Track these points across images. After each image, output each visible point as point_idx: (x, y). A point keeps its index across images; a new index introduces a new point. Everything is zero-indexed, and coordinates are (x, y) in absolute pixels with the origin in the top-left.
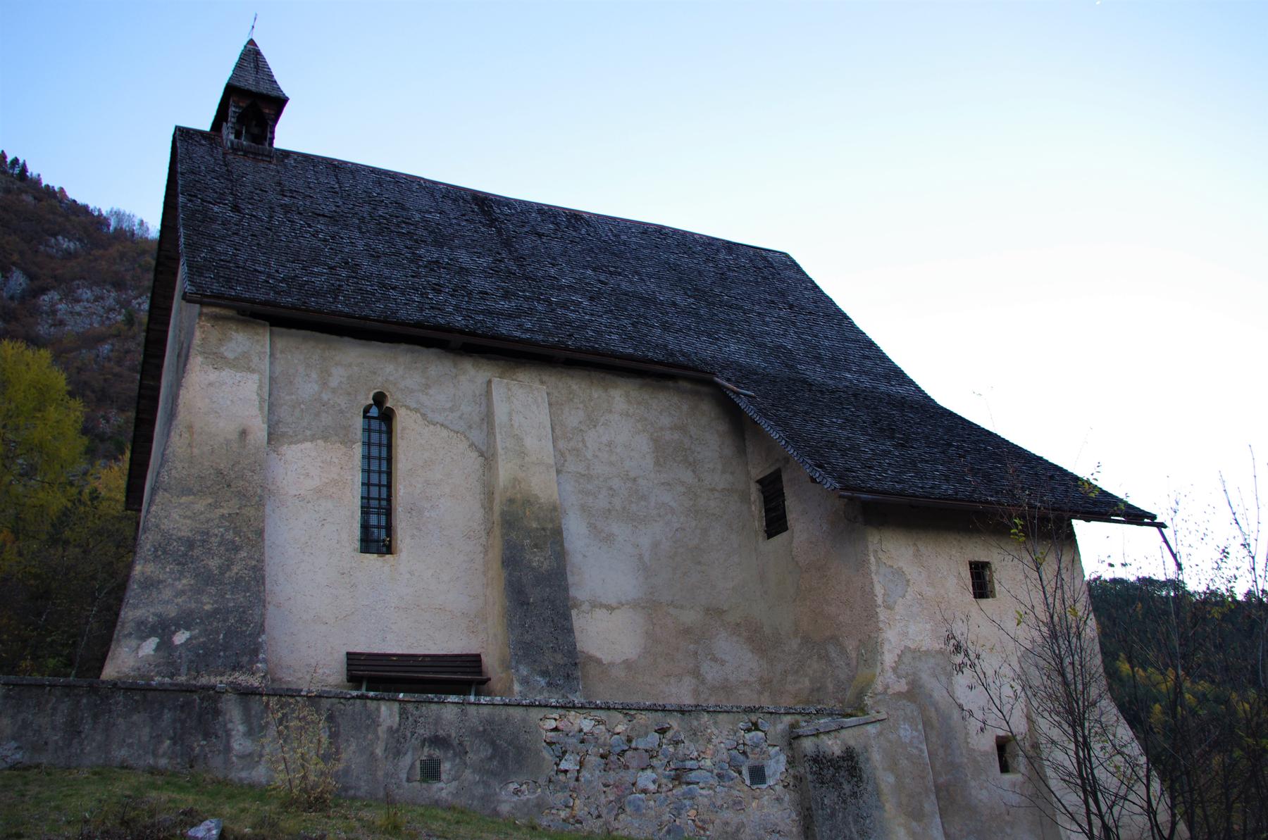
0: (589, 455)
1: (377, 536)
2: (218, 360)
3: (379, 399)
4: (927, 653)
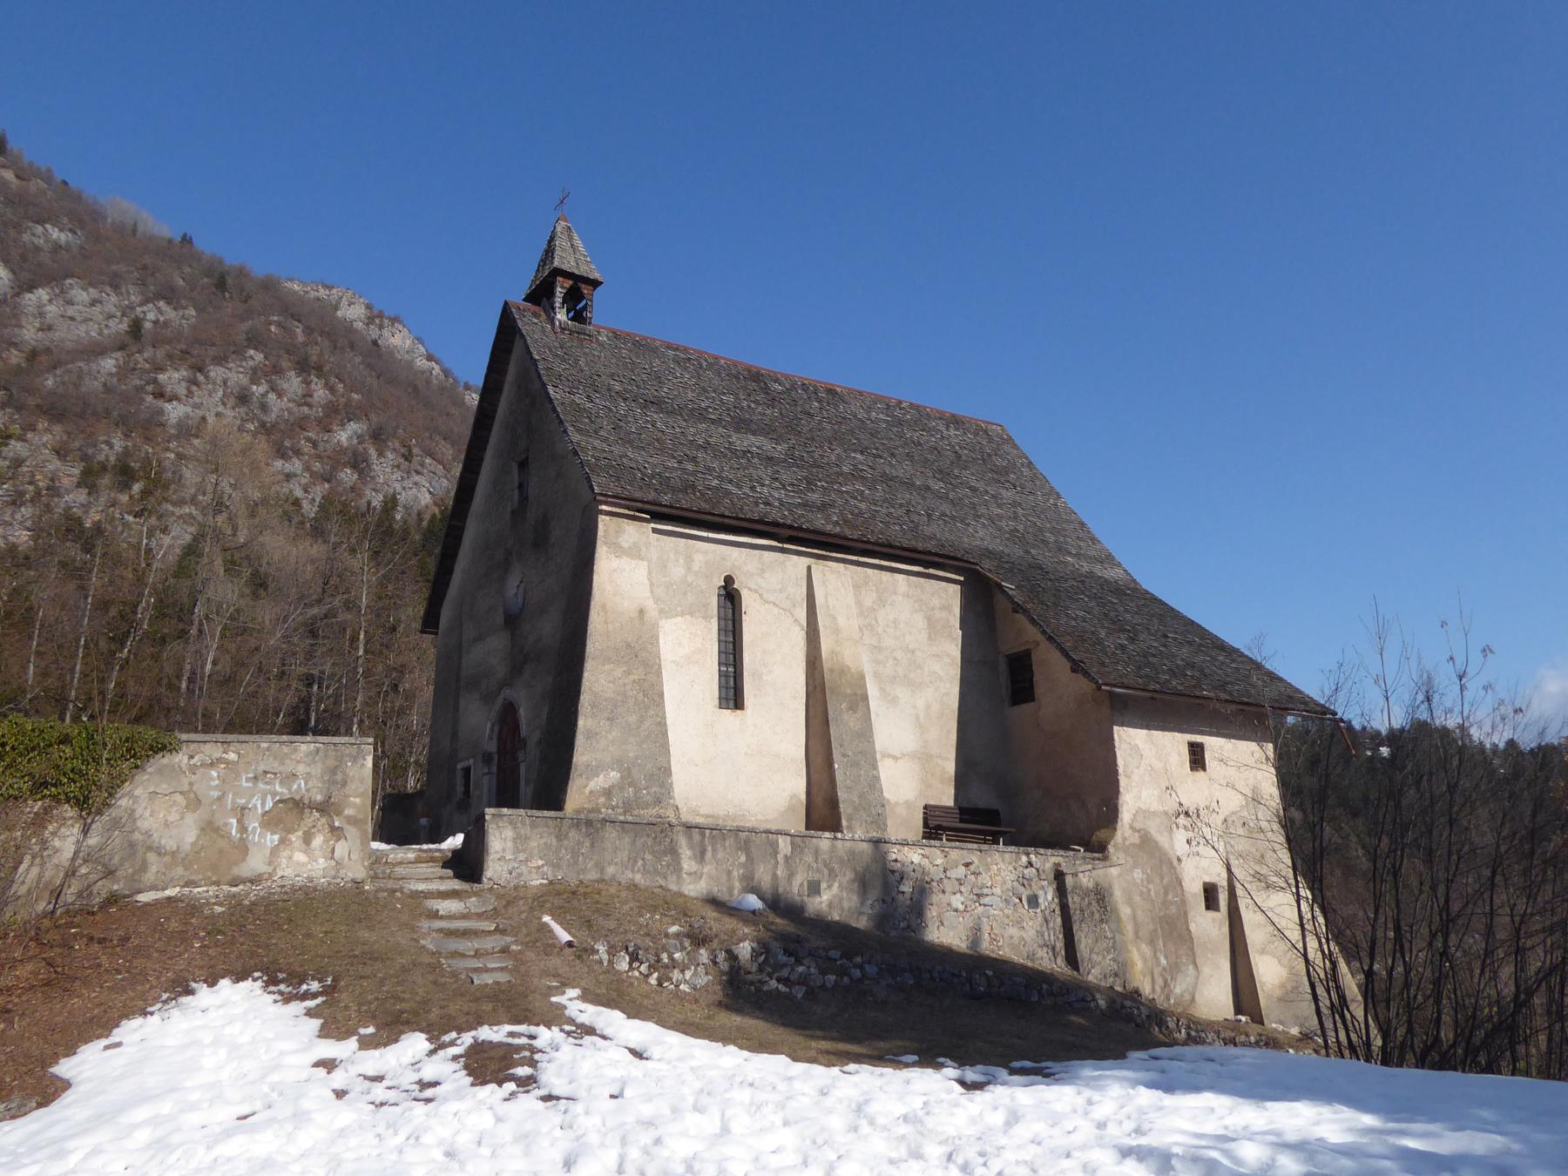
0: (880, 630)
1: (732, 694)
2: (619, 551)
3: (729, 580)
4: (1154, 813)
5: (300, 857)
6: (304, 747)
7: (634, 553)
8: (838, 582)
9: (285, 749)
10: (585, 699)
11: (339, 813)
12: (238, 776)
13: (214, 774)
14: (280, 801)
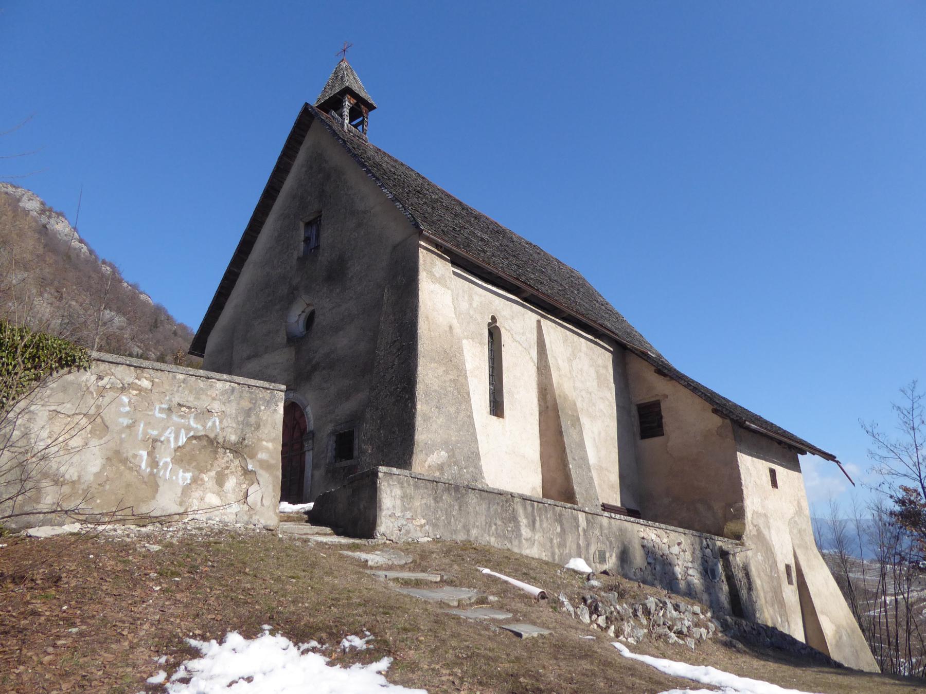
1: (497, 408)
5: (213, 499)
6: (219, 385)
7: (441, 281)
8: (557, 335)
9: (201, 384)
10: (420, 389)
11: (252, 457)
12: (151, 404)
13: (125, 399)
14: (194, 437)
